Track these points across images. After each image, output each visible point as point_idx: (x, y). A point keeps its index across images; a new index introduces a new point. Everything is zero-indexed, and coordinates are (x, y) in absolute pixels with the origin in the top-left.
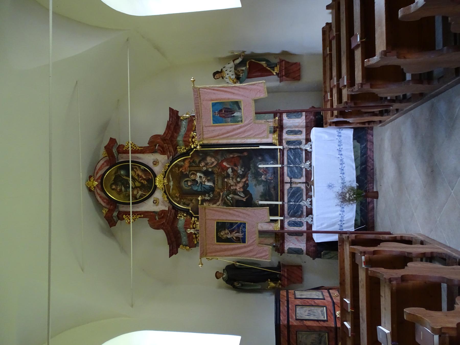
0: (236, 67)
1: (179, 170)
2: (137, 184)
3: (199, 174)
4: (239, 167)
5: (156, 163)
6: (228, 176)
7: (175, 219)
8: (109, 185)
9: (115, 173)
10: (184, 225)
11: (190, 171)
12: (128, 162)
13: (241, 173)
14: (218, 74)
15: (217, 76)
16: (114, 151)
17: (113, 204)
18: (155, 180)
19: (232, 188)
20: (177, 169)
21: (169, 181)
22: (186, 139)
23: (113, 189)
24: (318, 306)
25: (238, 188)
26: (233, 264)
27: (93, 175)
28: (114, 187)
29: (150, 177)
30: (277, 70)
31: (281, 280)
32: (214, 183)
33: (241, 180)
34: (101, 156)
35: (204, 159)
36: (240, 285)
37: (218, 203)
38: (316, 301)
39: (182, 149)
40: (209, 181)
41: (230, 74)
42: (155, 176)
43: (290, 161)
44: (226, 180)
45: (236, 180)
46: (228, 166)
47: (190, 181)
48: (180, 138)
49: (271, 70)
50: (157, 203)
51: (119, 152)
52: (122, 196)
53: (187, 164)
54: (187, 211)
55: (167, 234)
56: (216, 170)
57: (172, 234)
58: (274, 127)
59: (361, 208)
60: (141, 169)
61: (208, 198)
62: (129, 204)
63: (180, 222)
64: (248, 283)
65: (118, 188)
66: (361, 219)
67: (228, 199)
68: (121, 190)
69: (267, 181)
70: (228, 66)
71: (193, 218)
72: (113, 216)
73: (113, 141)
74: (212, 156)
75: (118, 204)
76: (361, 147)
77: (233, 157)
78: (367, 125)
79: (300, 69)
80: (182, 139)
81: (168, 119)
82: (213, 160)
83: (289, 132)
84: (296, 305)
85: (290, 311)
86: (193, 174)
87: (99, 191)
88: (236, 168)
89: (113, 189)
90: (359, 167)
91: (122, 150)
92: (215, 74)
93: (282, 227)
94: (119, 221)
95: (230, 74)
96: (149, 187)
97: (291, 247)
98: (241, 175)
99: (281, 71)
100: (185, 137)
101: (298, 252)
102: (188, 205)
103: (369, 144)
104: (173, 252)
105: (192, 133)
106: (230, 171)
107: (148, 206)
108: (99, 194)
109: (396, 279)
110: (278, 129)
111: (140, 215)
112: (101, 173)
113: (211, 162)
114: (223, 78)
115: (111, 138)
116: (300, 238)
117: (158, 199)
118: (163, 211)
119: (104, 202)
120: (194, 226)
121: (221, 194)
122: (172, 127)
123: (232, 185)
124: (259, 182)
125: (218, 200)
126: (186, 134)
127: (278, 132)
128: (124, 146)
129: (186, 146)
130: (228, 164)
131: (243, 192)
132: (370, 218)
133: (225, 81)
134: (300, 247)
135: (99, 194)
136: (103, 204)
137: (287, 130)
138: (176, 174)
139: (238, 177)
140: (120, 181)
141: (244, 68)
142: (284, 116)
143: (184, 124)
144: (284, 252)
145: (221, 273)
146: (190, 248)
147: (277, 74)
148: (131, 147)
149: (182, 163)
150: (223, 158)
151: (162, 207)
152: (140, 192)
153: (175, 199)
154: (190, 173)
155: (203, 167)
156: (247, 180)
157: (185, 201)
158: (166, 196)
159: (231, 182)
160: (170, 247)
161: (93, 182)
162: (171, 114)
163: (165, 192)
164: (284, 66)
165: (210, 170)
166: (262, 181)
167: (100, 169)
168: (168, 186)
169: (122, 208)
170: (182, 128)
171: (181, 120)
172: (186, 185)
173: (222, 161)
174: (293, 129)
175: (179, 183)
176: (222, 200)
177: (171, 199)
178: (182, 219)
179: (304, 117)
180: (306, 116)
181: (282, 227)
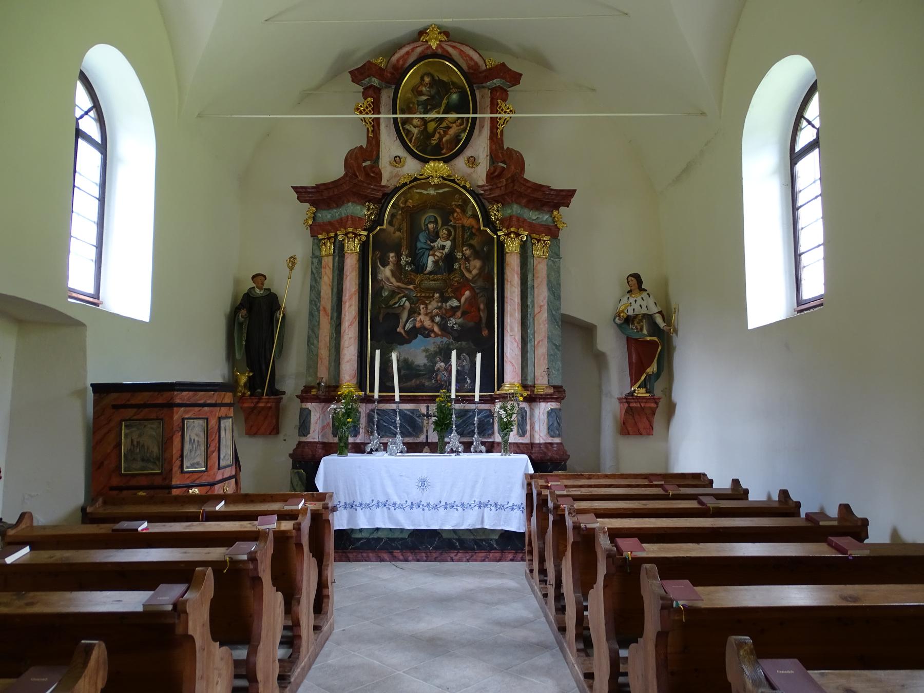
0: (649, 318)
1: (457, 206)
2: (431, 126)
3: (448, 244)
5: (472, 161)
6: (444, 299)
7: (363, 199)
9: (453, 83)
10: (352, 217)
11: (454, 227)
12: (475, 112)
15: (634, 281)
17: (395, 76)
18: (439, 160)
19: (422, 306)
20: (460, 203)
21: (437, 187)
23: (422, 79)
24: (207, 457)
25: (422, 317)
26: (279, 308)
28: (427, 80)
30: (641, 393)
31: (250, 395)
32: (431, 273)
35: (477, 254)
36: (241, 319)
37: (393, 280)
38: (215, 454)
39: (495, 213)
40: (436, 263)
42: (447, 161)
44: (437, 295)
45: (437, 315)
46: (463, 300)
48: (515, 210)
50: (396, 163)
51: (493, 90)
52: (410, 95)
53: (469, 222)
54: (379, 221)
55: (336, 183)
56: (456, 277)
61: (403, 262)
62: (395, 112)
63: (359, 207)
64: (245, 335)
65: (424, 89)
66: (361, 539)
67: (401, 298)
68: (421, 93)
70: (651, 302)
71: (365, 233)
73: (515, 78)
74: (481, 269)
77: (479, 309)
82: (475, 272)
84: (207, 419)
85: (197, 409)
86: (449, 234)
87: (419, 50)
88: (459, 314)
89: (422, 79)
91: (499, 96)
92: (637, 277)
94: (361, 89)
95: (636, 306)
96: (426, 147)
97: (312, 414)
100: (518, 219)
101: (304, 427)
102: (390, 223)
104: (302, 193)
105: (526, 233)
106: (454, 303)
107: (390, 146)
108: (413, 49)
115: (521, 75)
117: (403, 166)
118: (379, 175)
119: (398, 61)
120: (351, 235)
121: (411, 287)
122: (538, 195)
124: (432, 357)
128: (505, 100)
129: (502, 221)
130: (466, 299)
132: (365, 555)
134: (312, 430)
135: (413, 49)
136: (394, 59)
137: (528, 409)
138: (448, 201)
139: (442, 318)
140: (438, 93)
141: (645, 332)
145: (263, 284)
146: (310, 226)
149: (470, 213)
150: (477, 291)
151: (389, 175)
152: (415, 131)
153: (403, 199)
155: (462, 252)
156: (437, 335)
157: (399, 217)
158: (408, 181)
159: (433, 305)
160: (313, 188)
161: (436, 39)
163: (416, 179)
165: (456, 266)
168: (427, 185)
169: (386, 97)
172: (429, 221)
173: (472, 289)
174: (528, 422)
175: (432, 207)
176: (399, 287)
177: (402, 191)
178: (363, 211)
180: (551, 444)
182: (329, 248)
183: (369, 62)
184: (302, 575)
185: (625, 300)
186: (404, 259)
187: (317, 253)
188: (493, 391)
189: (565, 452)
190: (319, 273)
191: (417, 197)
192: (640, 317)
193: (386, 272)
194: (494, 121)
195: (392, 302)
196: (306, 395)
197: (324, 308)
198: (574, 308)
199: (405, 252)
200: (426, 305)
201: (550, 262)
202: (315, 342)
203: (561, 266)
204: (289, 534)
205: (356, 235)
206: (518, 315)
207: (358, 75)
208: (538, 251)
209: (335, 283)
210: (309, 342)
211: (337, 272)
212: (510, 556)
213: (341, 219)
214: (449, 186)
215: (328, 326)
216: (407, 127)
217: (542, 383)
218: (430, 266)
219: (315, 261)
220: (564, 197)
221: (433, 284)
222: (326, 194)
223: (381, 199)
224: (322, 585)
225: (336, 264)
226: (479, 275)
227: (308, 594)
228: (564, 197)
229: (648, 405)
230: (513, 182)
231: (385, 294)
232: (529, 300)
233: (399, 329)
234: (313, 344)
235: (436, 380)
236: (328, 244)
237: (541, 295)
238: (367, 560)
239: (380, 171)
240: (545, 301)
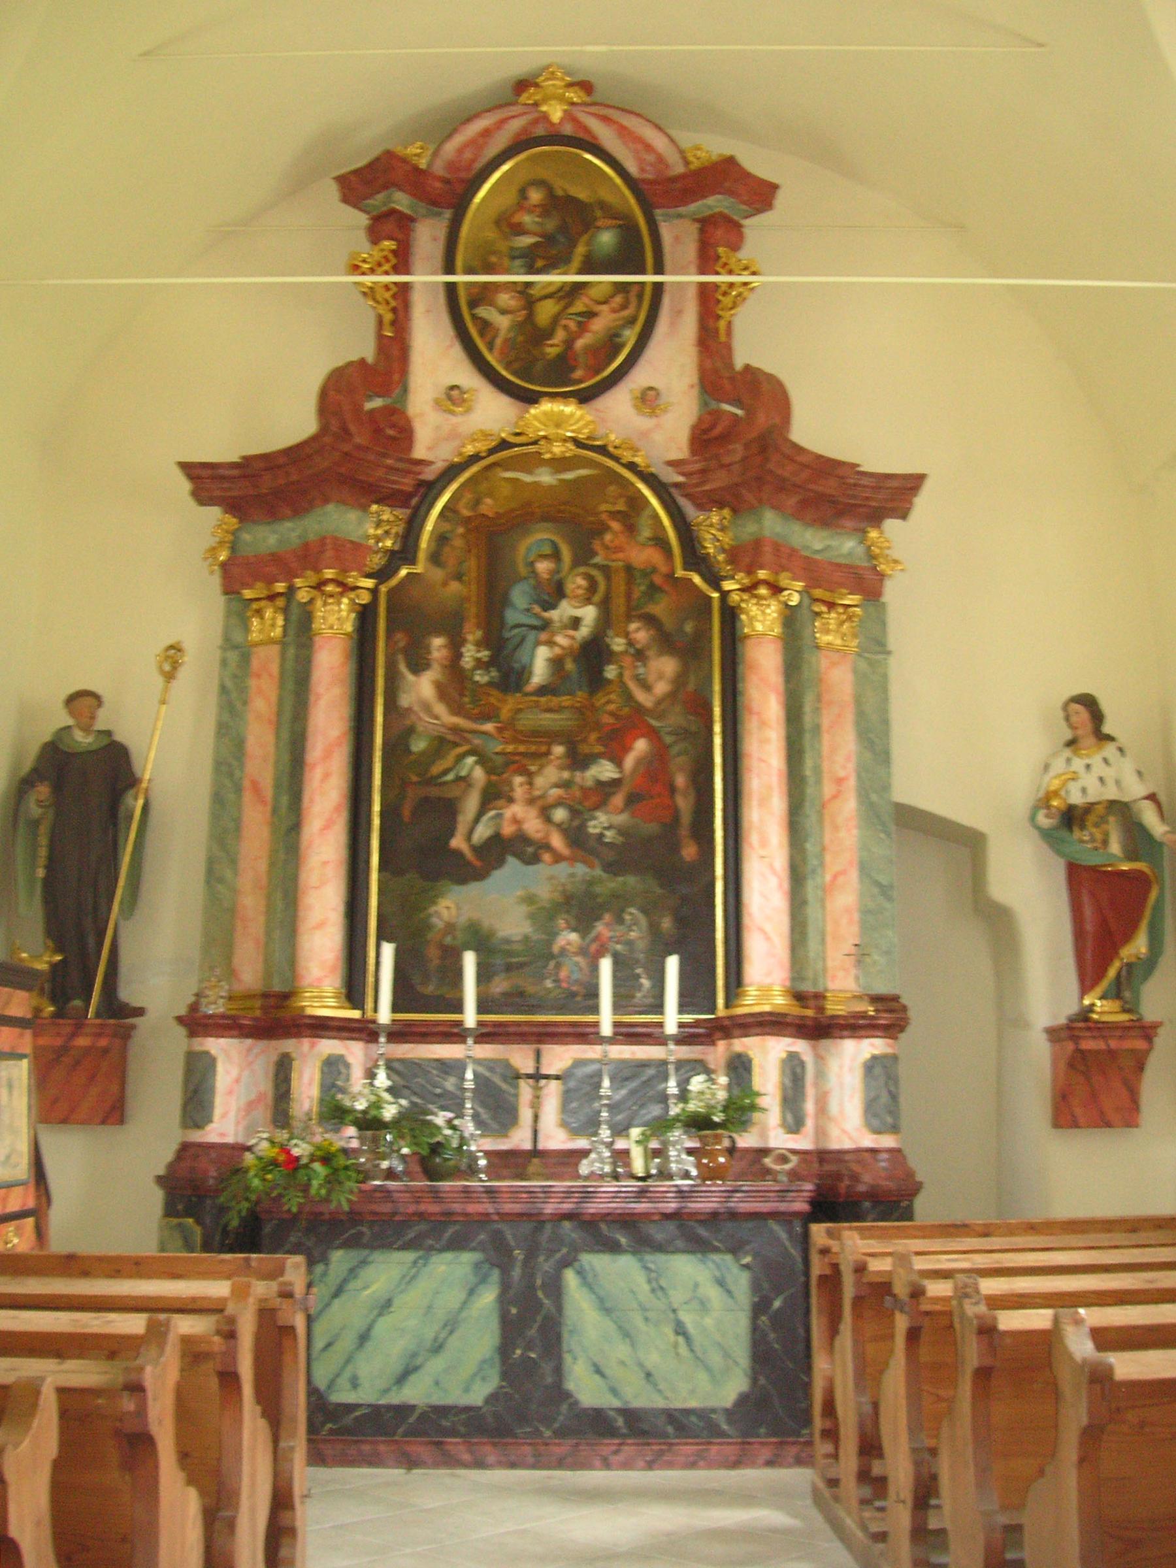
0: (1121, 809)
1: (614, 515)
2: (546, 311)
3: (589, 614)
4: (622, 819)
5: (648, 400)
6: (578, 760)
7: (367, 492)
8: (542, 173)
9: (603, 205)
10: (335, 539)
11: (605, 570)
12: (659, 270)
13: (593, 828)
14: (1087, 719)
15: (1081, 714)
16: (711, 201)
17: (453, 195)
18: (565, 396)
19: (518, 780)
20: (621, 506)
21: (561, 464)
22: (768, 555)
25: (516, 809)
26: (133, 781)
27: (597, 97)
29: (578, 374)
30: (1102, 1008)
31: (58, 1015)
32: (542, 690)
33: (559, 826)
34: (687, 139)
35: (666, 642)
36: (35, 811)
37: (440, 709)
39: (715, 531)
40: (556, 663)
41: (1090, 781)
42: (585, 397)
43: (651, 1072)
44: (559, 750)
45: (559, 803)
46: (629, 761)
47: (557, 571)
48: (771, 524)
49: (1105, 984)
50: (451, 407)
51: (706, 224)
52: (491, 234)
53: (643, 556)
54: (405, 552)
55: (295, 454)
56: (609, 704)
57: (294, 478)
58: (819, 997)
59: (413, 1408)
60: (623, 326)
61: (467, 661)
62: (449, 269)
63: (352, 515)
64: (43, 852)
66: (356, 1406)
67: (461, 757)
68: (519, 230)
69: (552, 956)
70: (1126, 769)
71: (369, 583)
72: (395, 192)
73: (762, 195)
74: (679, 681)
75: (448, 214)
76: (713, 1411)
77: (672, 789)
78: (818, 1423)
79: (1109, 1125)
80: (767, 533)
81: (868, 467)
82: (661, 688)
83: (793, 1069)
86: (592, 587)
87: (515, 125)
88: (618, 800)
89: (523, 193)
90: (617, 1403)
91: (717, 241)
92: (1089, 703)
93: (322, 1027)
94: (363, 219)
95: (1090, 781)
96: (531, 365)
97: (220, 1068)
98: (582, 827)
99: (1102, 1029)
100: (777, 548)
101: (197, 1102)
102: (435, 558)
103: (731, 1451)
104: (206, 480)
105: (799, 585)
106: (605, 770)
107: (434, 357)
108: (503, 122)
109: (141, 1411)
110: (810, 1013)
111: (393, 323)
112: (606, 136)
113: (651, 678)
114: (1071, 743)
115: (774, 187)
116: (263, 1114)
117: (469, 410)
118: (405, 434)
119: (460, 151)
120: (330, 588)
121: (489, 727)
122: (829, 486)
123: (530, 784)
124: (546, 917)
125: (457, 710)
126: (793, 552)
127: (796, 1010)
128: (735, 247)
129: (734, 555)
130: (638, 762)
131: (496, 838)
132: (366, 1448)
133: (1055, 754)
134: (217, 1112)
135: (503, 122)
136: (450, 148)
137: (808, 1057)
138: (590, 504)
139: (574, 813)
140: (564, 226)
141: (1115, 847)
142: (878, 1042)
143: (844, 546)
144: (192, 1034)
145: (93, 718)
146: (224, 565)
147: (1085, 1015)
148: (731, 285)
149: (646, 533)
150: (668, 739)
151: (434, 436)
152: (503, 323)
154: (594, 572)
155: (627, 635)
156: (558, 858)
157: (458, 543)
158: (482, 447)
159: (549, 777)
160: (233, 465)
161: (561, 99)
162: (895, 484)
163: (504, 445)
164: (1128, 1044)
165: (611, 672)
166: (553, 934)
167: (623, 132)
168: (531, 462)
169: (428, 237)
170: (824, 533)
171: (864, 532)
172: (536, 553)
173: (653, 734)
174: (810, 1092)
175: (546, 518)
176: (455, 729)
177: (466, 475)
178: (372, 527)
179: (868, 1141)
180: (873, 1151)
181: (322, 1027)
182: (270, 624)
183: (389, 154)
184: (239, 1460)
185: (1059, 765)
186: (470, 654)
187: (238, 637)
188: (712, 1009)
189: (910, 1174)
190: (243, 690)
191: (506, 490)
192: (1100, 809)
193: (422, 688)
194: (707, 294)
195: (435, 770)
196: (196, 1023)
197: (256, 788)
198: (919, 784)
199: (473, 635)
200: (530, 775)
201: (863, 665)
202: (228, 874)
203: (893, 674)
204: (204, 1347)
205: (347, 588)
206: (778, 804)
207: (357, 186)
208: (830, 633)
209: (287, 715)
210: (212, 876)
211: (290, 686)
212: (766, 1453)
213: (306, 546)
214: (590, 463)
215: (265, 832)
216: (483, 312)
217: (843, 985)
218: (540, 669)
219: (233, 656)
220: (894, 495)
221: (547, 720)
222: (267, 483)
223: (410, 495)
224: (282, 1501)
225: (290, 664)
226: (672, 696)
227: (253, 1510)
228: (894, 495)
229: (1128, 1044)
230: (763, 450)
231: (419, 745)
232: (809, 763)
233: (457, 842)
234: (221, 880)
235: (557, 981)
236: (268, 614)
237: (839, 751)
238: (374, 1461)
239: (408, 421)
240: (851, 766)
